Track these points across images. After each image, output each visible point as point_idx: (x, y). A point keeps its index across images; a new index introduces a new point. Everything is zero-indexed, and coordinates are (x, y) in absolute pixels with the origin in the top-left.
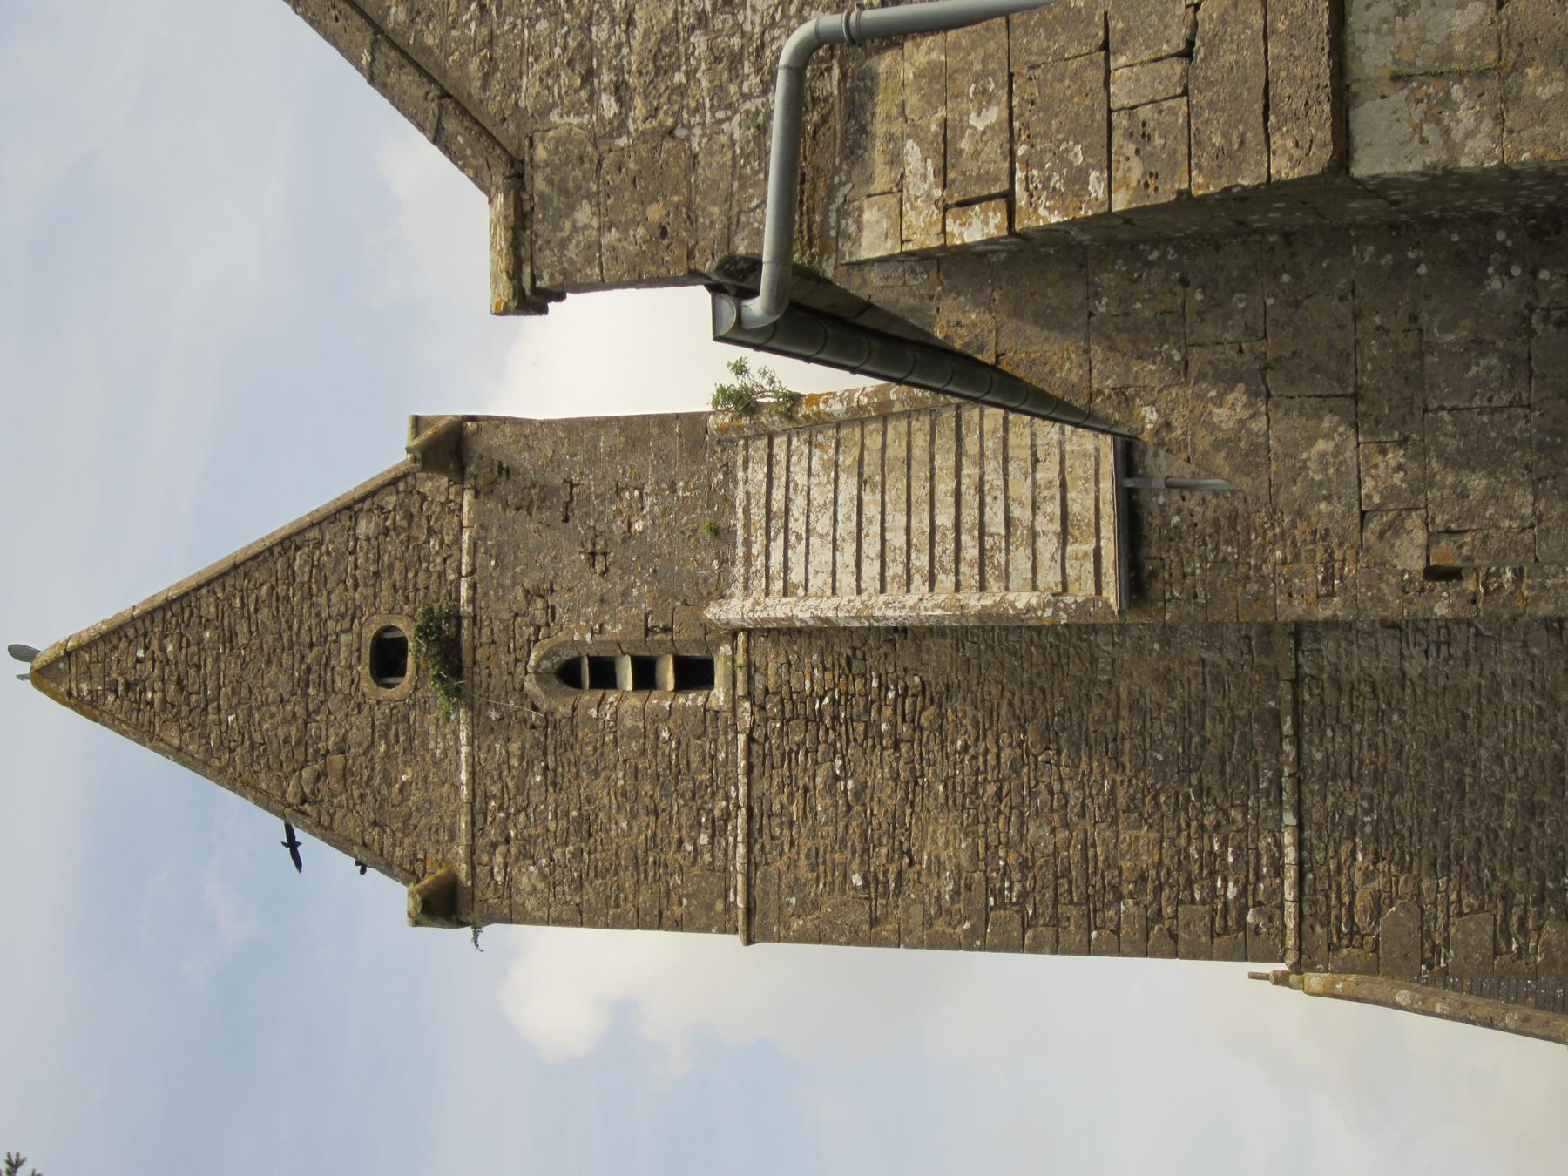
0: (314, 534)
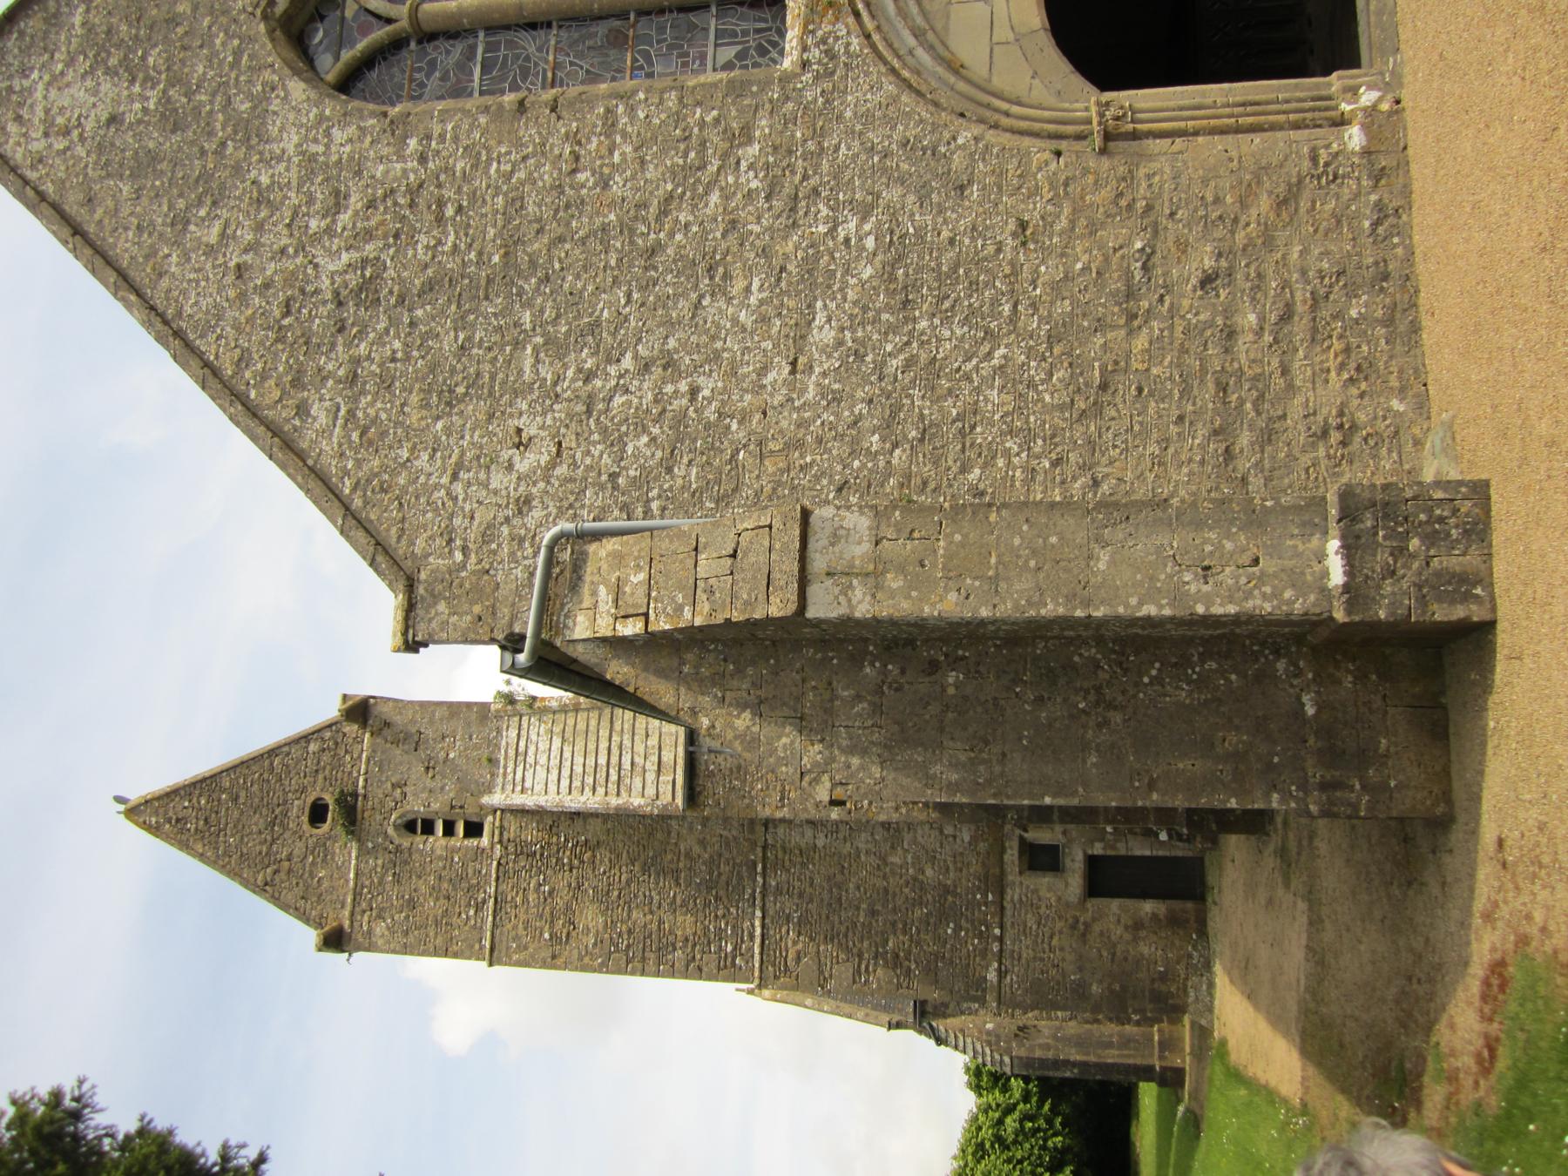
0: (286, 749)
